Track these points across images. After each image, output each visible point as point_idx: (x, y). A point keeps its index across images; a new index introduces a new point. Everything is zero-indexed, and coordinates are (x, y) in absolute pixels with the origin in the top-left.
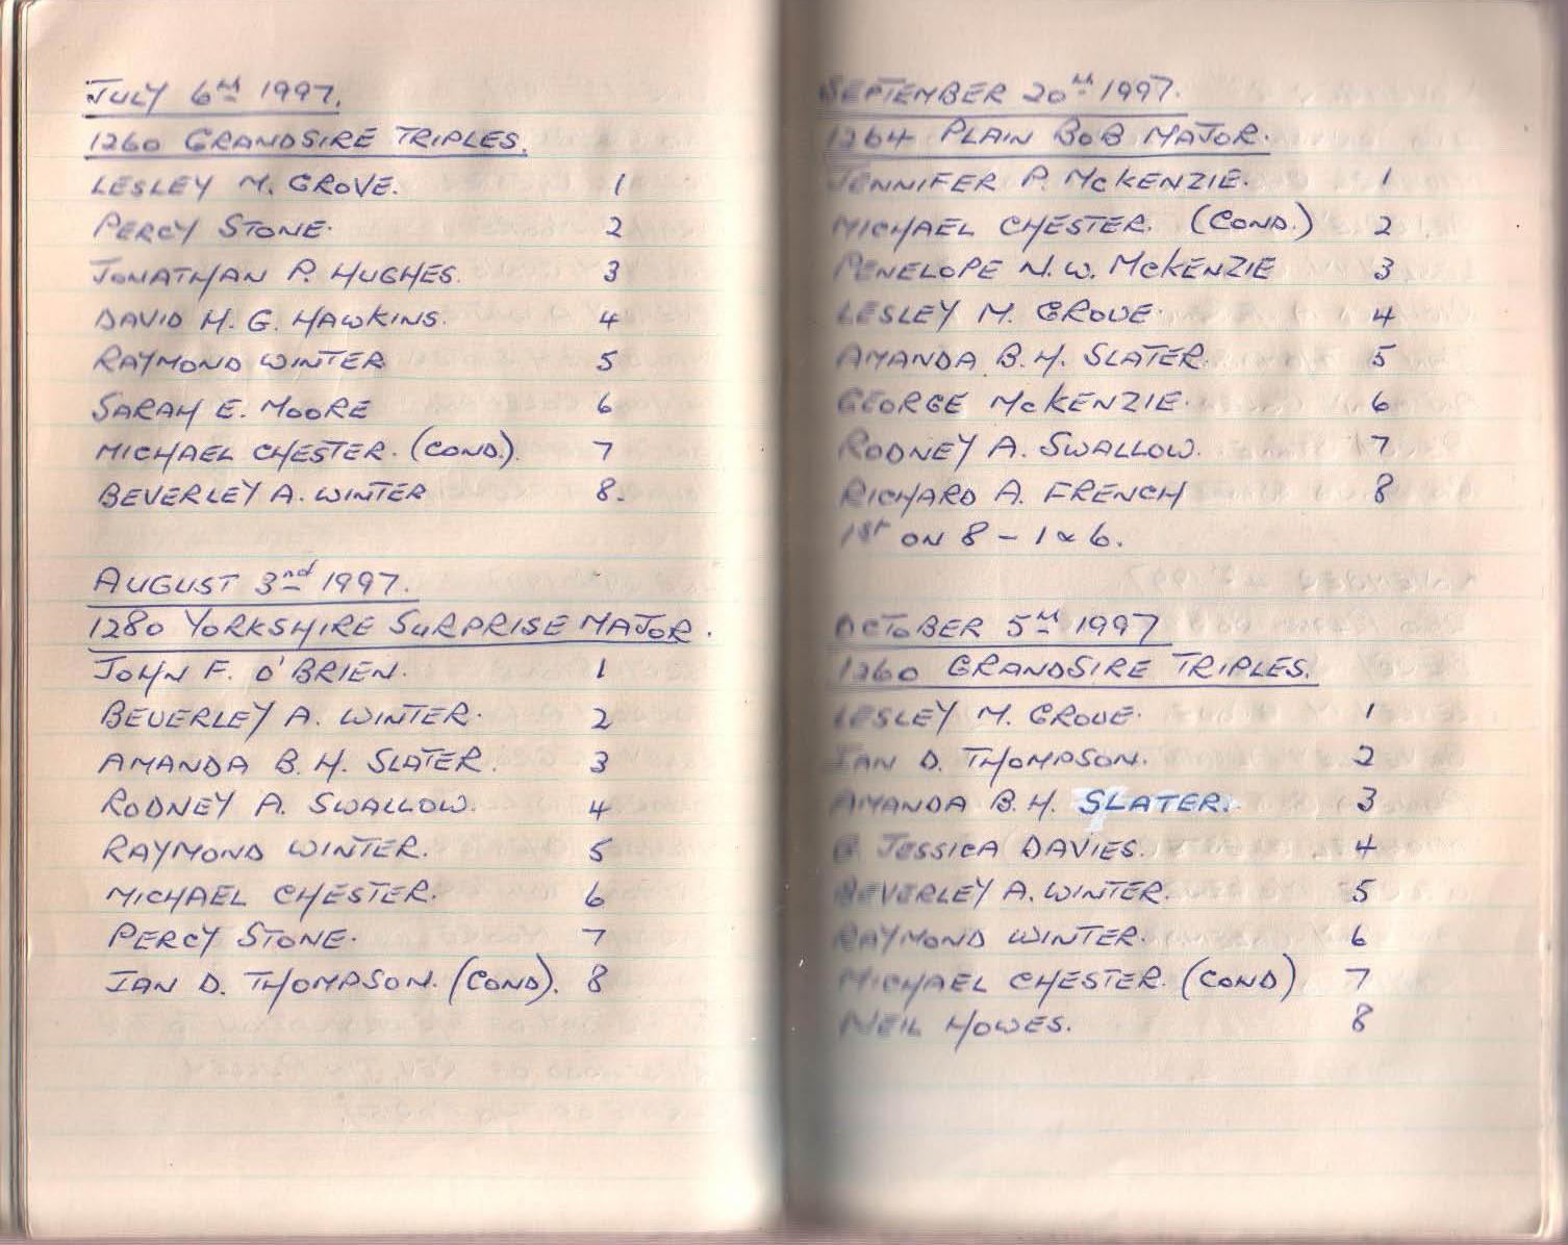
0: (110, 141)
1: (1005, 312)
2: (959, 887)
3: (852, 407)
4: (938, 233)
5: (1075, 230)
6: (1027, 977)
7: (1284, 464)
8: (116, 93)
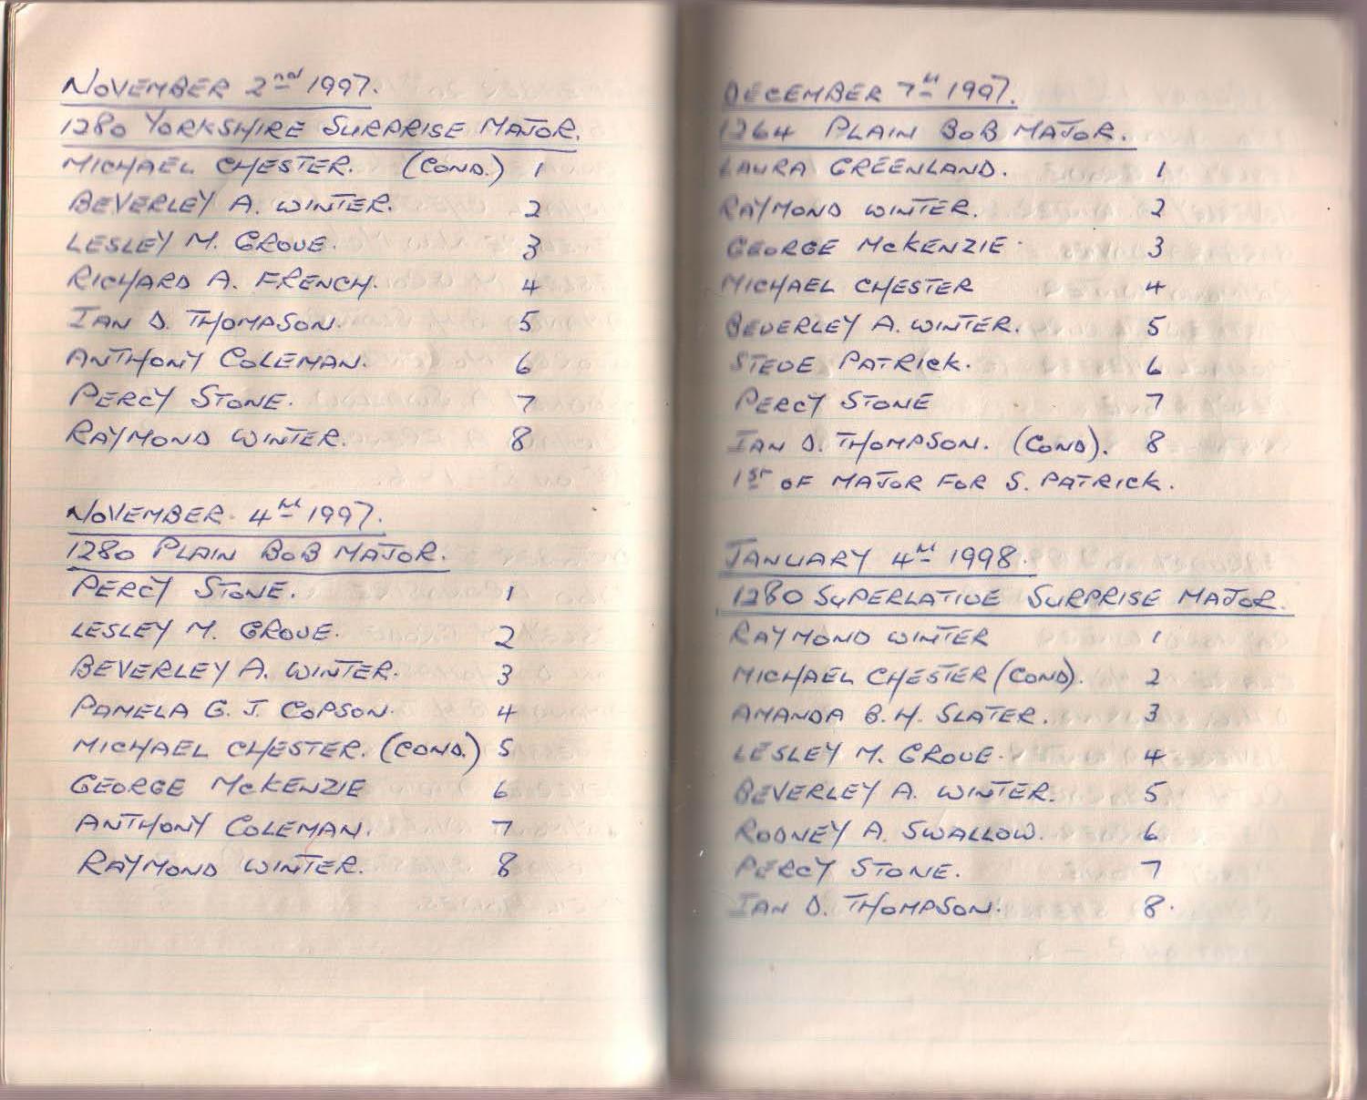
1: (209, 628)
5: (203, 401)
7: (1243, 539)
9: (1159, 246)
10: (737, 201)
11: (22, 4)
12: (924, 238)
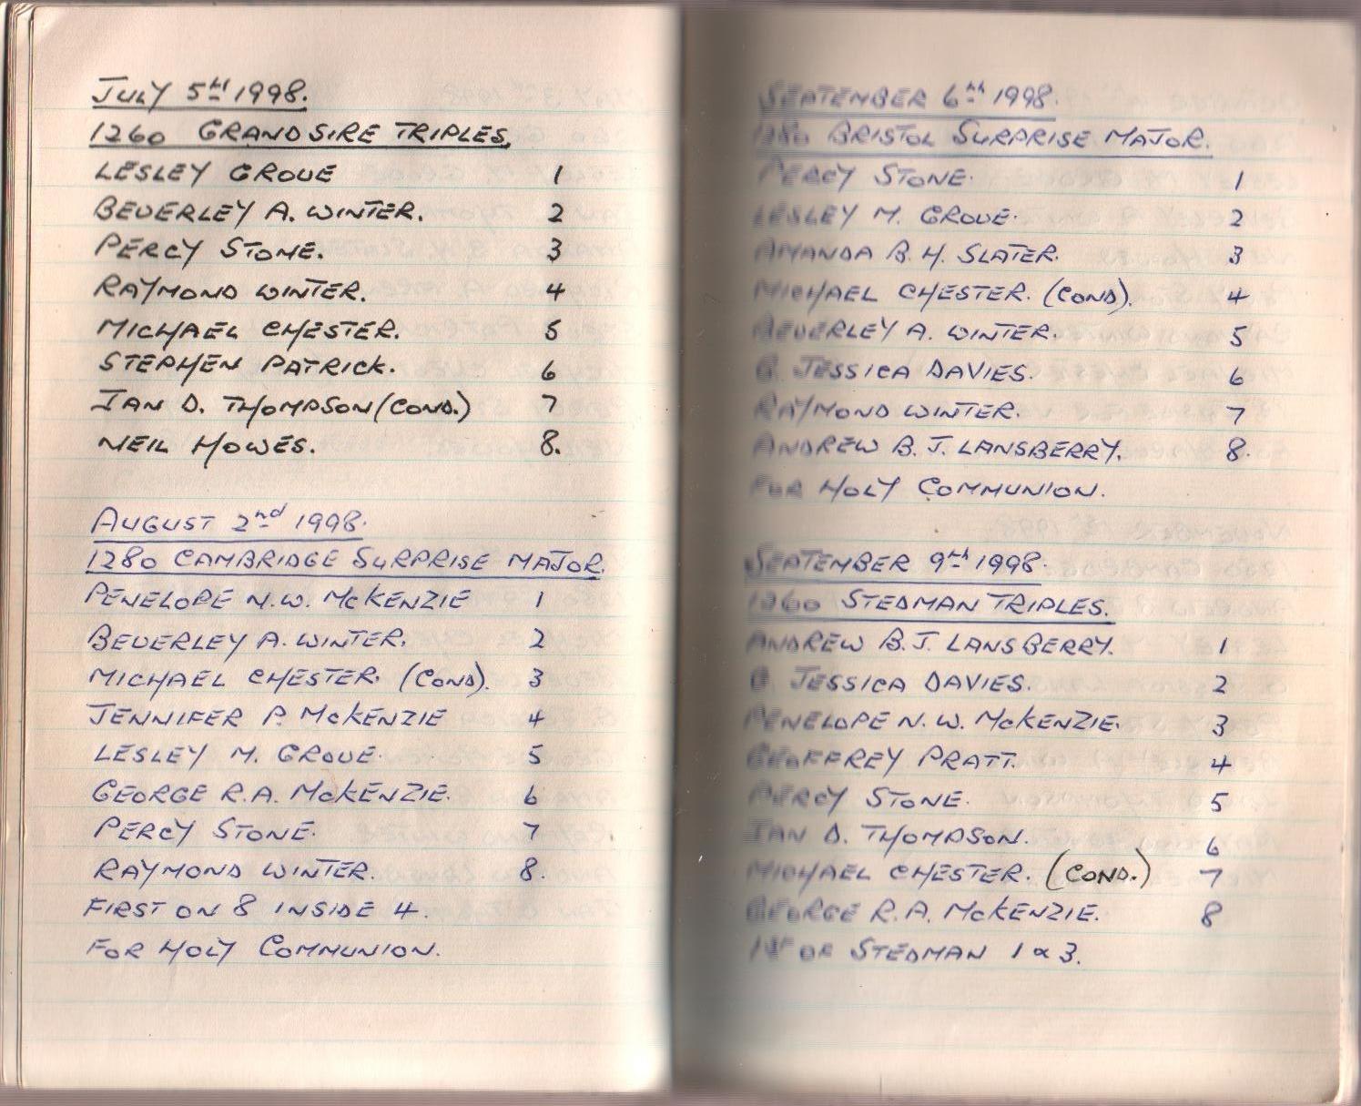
0: (113, 132)
2: (866, 325)
3: (760, 761)
4: (843, 876)
6: (259, 673)
8: (123, 92)
9: (1070, 954)
10: (775, 400)
11: (22, 5)
12: (366, 709)
